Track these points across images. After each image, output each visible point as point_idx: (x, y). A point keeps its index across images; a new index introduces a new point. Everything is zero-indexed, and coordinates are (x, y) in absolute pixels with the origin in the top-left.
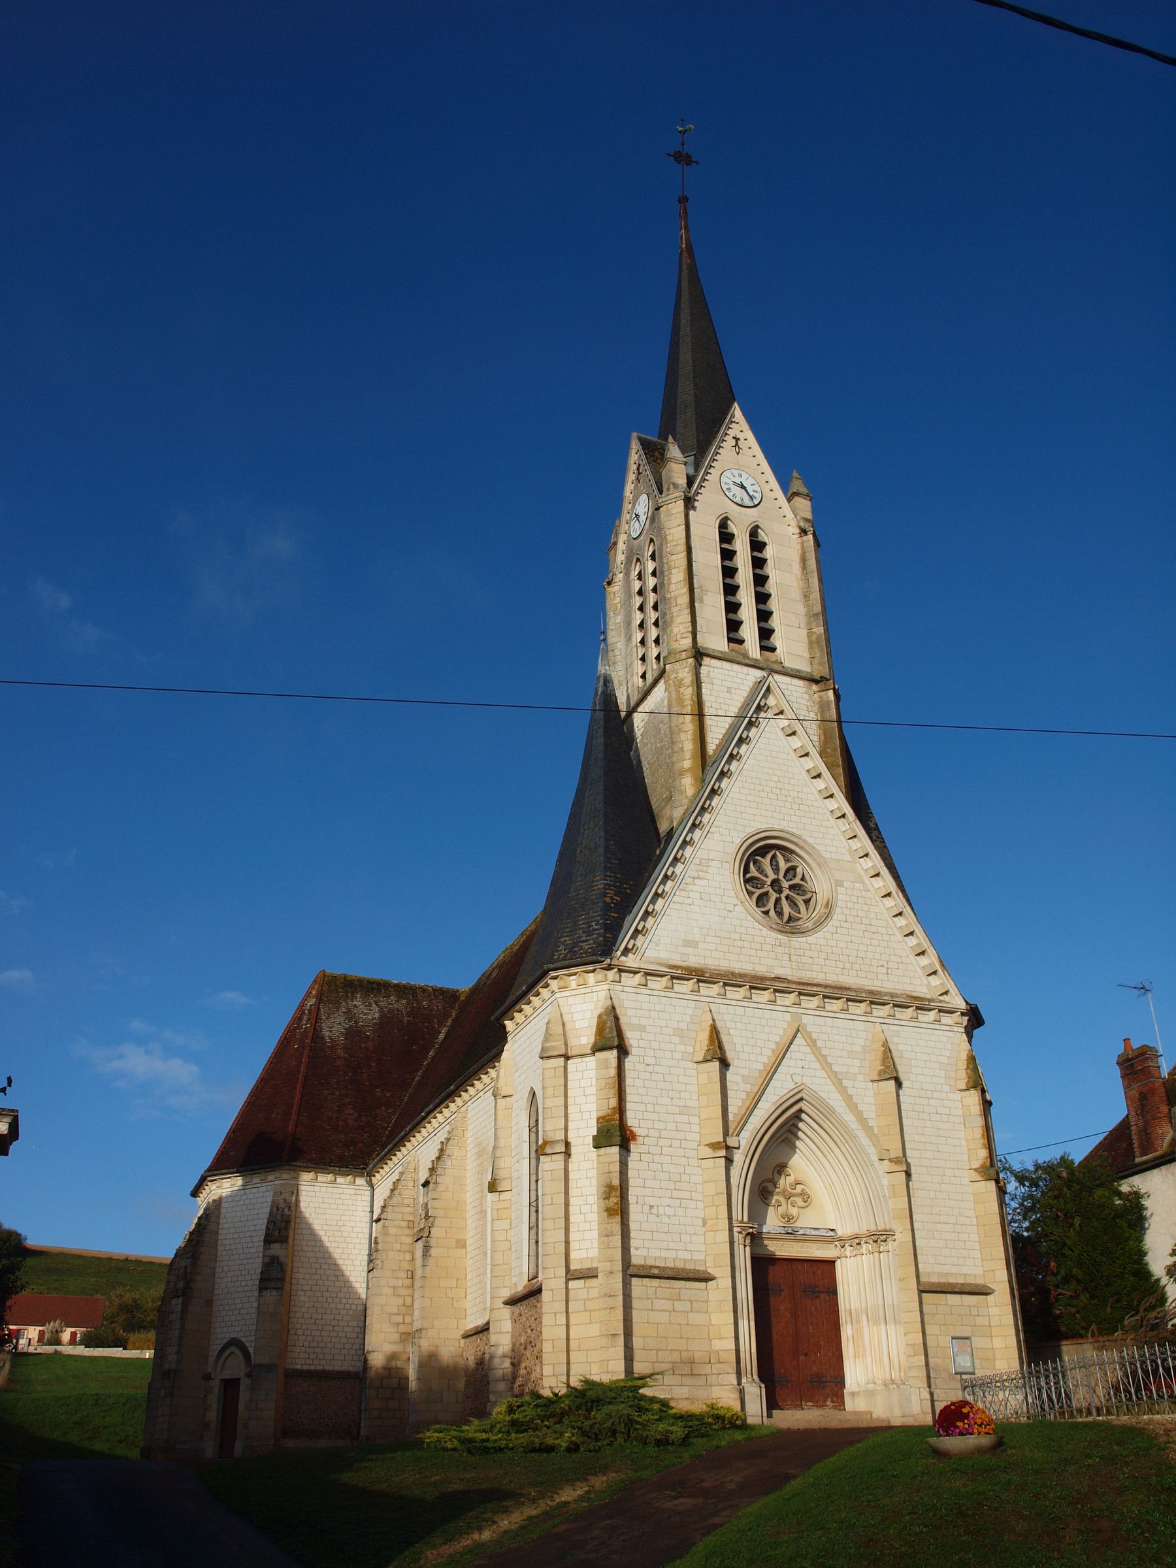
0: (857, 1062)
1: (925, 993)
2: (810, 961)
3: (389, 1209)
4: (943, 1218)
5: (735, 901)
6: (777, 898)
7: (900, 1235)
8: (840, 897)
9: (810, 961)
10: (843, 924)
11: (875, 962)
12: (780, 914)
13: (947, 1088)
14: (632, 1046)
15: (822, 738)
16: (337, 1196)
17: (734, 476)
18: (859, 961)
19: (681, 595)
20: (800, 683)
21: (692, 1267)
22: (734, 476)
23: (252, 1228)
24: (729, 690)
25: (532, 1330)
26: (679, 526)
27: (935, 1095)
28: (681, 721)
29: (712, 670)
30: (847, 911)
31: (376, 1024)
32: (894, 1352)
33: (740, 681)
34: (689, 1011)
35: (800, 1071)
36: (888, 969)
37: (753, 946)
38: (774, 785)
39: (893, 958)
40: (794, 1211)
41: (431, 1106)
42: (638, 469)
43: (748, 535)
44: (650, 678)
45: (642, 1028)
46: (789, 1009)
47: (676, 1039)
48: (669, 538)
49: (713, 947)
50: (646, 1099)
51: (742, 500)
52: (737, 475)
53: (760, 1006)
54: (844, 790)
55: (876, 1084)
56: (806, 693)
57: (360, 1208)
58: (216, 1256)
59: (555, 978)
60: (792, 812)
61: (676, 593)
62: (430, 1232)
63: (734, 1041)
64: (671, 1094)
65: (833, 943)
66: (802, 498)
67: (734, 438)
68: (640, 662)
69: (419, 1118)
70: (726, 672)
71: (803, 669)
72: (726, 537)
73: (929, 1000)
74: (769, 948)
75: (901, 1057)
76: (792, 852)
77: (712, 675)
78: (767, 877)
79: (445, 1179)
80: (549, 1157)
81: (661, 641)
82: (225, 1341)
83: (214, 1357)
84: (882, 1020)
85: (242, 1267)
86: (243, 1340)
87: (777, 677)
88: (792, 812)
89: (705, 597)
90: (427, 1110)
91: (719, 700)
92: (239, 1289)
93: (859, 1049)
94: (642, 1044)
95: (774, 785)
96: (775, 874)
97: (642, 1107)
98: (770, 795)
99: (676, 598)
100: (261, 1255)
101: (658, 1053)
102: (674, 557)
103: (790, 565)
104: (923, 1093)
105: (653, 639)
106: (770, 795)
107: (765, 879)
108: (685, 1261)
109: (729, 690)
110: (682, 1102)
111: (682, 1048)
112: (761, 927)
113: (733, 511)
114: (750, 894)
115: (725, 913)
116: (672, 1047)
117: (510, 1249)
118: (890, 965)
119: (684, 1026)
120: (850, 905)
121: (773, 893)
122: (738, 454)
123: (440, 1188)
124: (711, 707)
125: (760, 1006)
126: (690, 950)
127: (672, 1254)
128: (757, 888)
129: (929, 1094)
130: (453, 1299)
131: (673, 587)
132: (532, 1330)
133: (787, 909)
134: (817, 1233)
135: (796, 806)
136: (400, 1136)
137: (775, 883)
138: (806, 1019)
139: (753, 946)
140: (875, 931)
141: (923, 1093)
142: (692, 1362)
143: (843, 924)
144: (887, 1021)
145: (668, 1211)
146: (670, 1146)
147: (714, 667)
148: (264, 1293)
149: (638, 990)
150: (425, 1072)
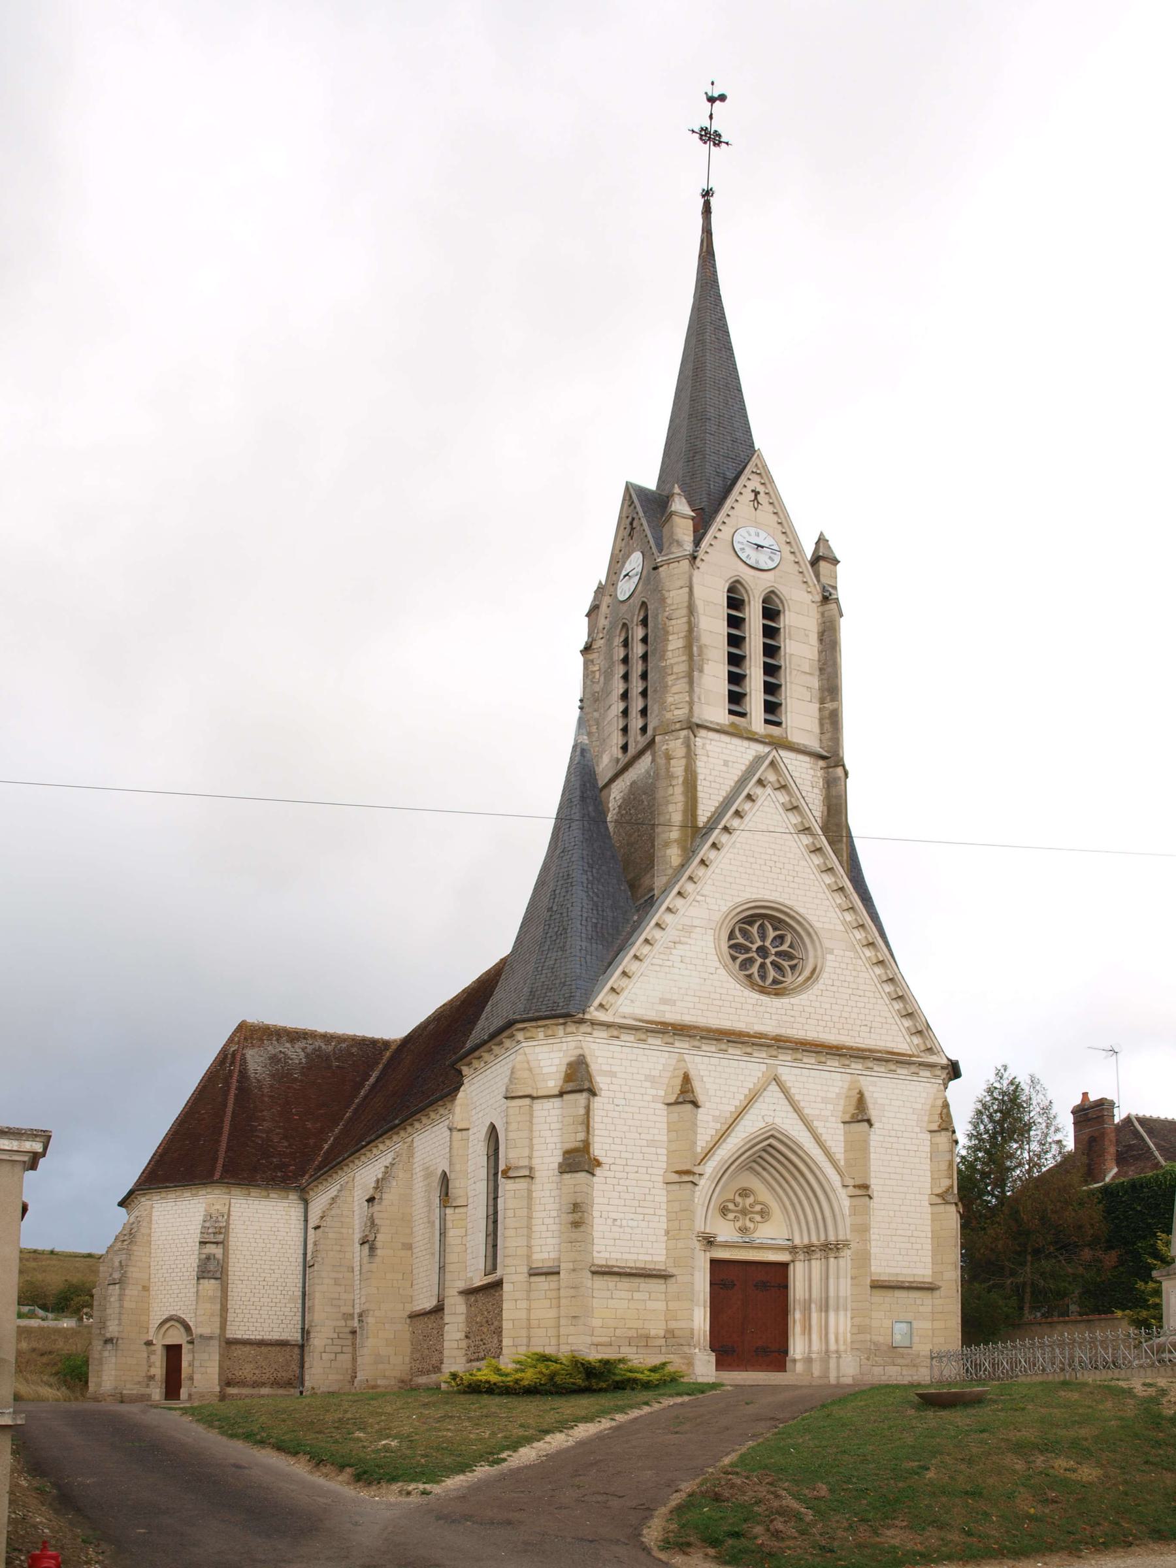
0: (830, 1107)
1: (906, 1050)
2: (792, 1019)
3: (328, 1219)
4: (899, 1232)
5: (718, 964)
6: (761, 963)
7: (856, 1245)
8: (828, 964)
9: (792, 1019)
10: (829, 988)
11: (859, 1022)
12: (763, 977)
13: (917, 1129)
14: (601, 1089)
15: (826, 813)
16: (271, 1208)
17: (750, 535)
18: (843, 1020)
19: (678, 663)
20: (807, 759)
21: (652, 1266)
22: (750, 535)
23: (186, 1232)
24: (726, 763)
25: (489, 1312)
26: (682, 588)
27: (905, 1134)
28: (671, 792)
29: (708, 742)
30: (835, 977)
31: (303, 1068)
32: (841, 1330)
33: (739, 755)
34: (663, 1061)
35: (772, 1113)
36: (871, 1028)
37: (733, 1004)
38: (768, 857)
39: (878, 1019)
40: (750, 1225)
41: (373, 1137)
42: (631, 524)
43: (761, 601)
44: (632, 751)
45: (613, 1074)
46: (766, 1061)
47: (648, 1084)
48: (669, 601)
49: (691, 1005)
50: (613, 1134)
51: (757, 562)
52: (753, 534)
53: (736, 1057)
54: (846, 869)
55: (847, 1125)
56: (811, 769)
57: (293, 1218)
58: (150, 1253)
59: (523, 1029)
60: (786, 884)
61: (672, 661)
62: (376, 1237)
63: (707, 1087)
64: (640, 1130)
65: (817, 1004)
66: (829, 562)
67: (753, 491)
68: (620, 733)
69: (359, 1146)
70: (724, 745)
71: (806, 742)
72: (735, 602)
73: (910, 1056)
74: (750, 1007)
75: (875, 1103)
76: (780, 921)
77: (708, 747)
78: (752, 943)
79: (390, 1196)
80: (512, 1181)
81: (649, 712)
82: (164, 1317)
83: (154, 1329)
84: (859, 1072)
85: (177, 1262)
86: (183, 1316)
87: (783, 753)
88: (786, 884)
89: (705, 666)
90: (368, 1140)
91: (714, 773)
92: (175, 1279)
93: (834, 1096)
94: (612, 1087)
95: (768, 857)
96: (761, 941)
97: (610, 1140)
98: (764, 868)
99: (672, 665)
100: (197, 1252)
101: (628, 1096)
102: (673, 622)
103: (807, 636)
104: (893, 1133)
105: (640, 708)
106: (764, 868)
107: (750, 945)
108: (924, 1276)
109: (726, 763)
110: (650, 1137)
111: (654, 1092)
112: (742, 988)
113: (747, 575)
114: (734, 958)
115: (706, 976)
116: (643, 1091)
117: (466, 1251)
118: (874, 1024)
119: (654, 1073)
120: (839, 971)
121: (758, 958)
122: (756, 509)
123: (385, 1203)
124: (705, 779)
125: (736, 1057)
126: (667, 1008)
127: (634, 1257)
128: (740, 953)
129: (900, 1134)
130: (399, 1288)
131: (669, 654)
132: (489, 1312)
133: (772, 973)
134: (773, 1242)
135: (790, 878)
136: (338, 1160)
137: (763, 951)
138: (781, 1070)
139: (733, 1004)
140: (862, 994)
141: (893, 1133)
142: (647, 1337)
143: (829, 988)
144: (864, 1073)
145: (631, 1223)
146: (637, 1172)
147: (711, 740)
148: (202, 1281)
149: (610, 1042)
150: (355, 1109)
